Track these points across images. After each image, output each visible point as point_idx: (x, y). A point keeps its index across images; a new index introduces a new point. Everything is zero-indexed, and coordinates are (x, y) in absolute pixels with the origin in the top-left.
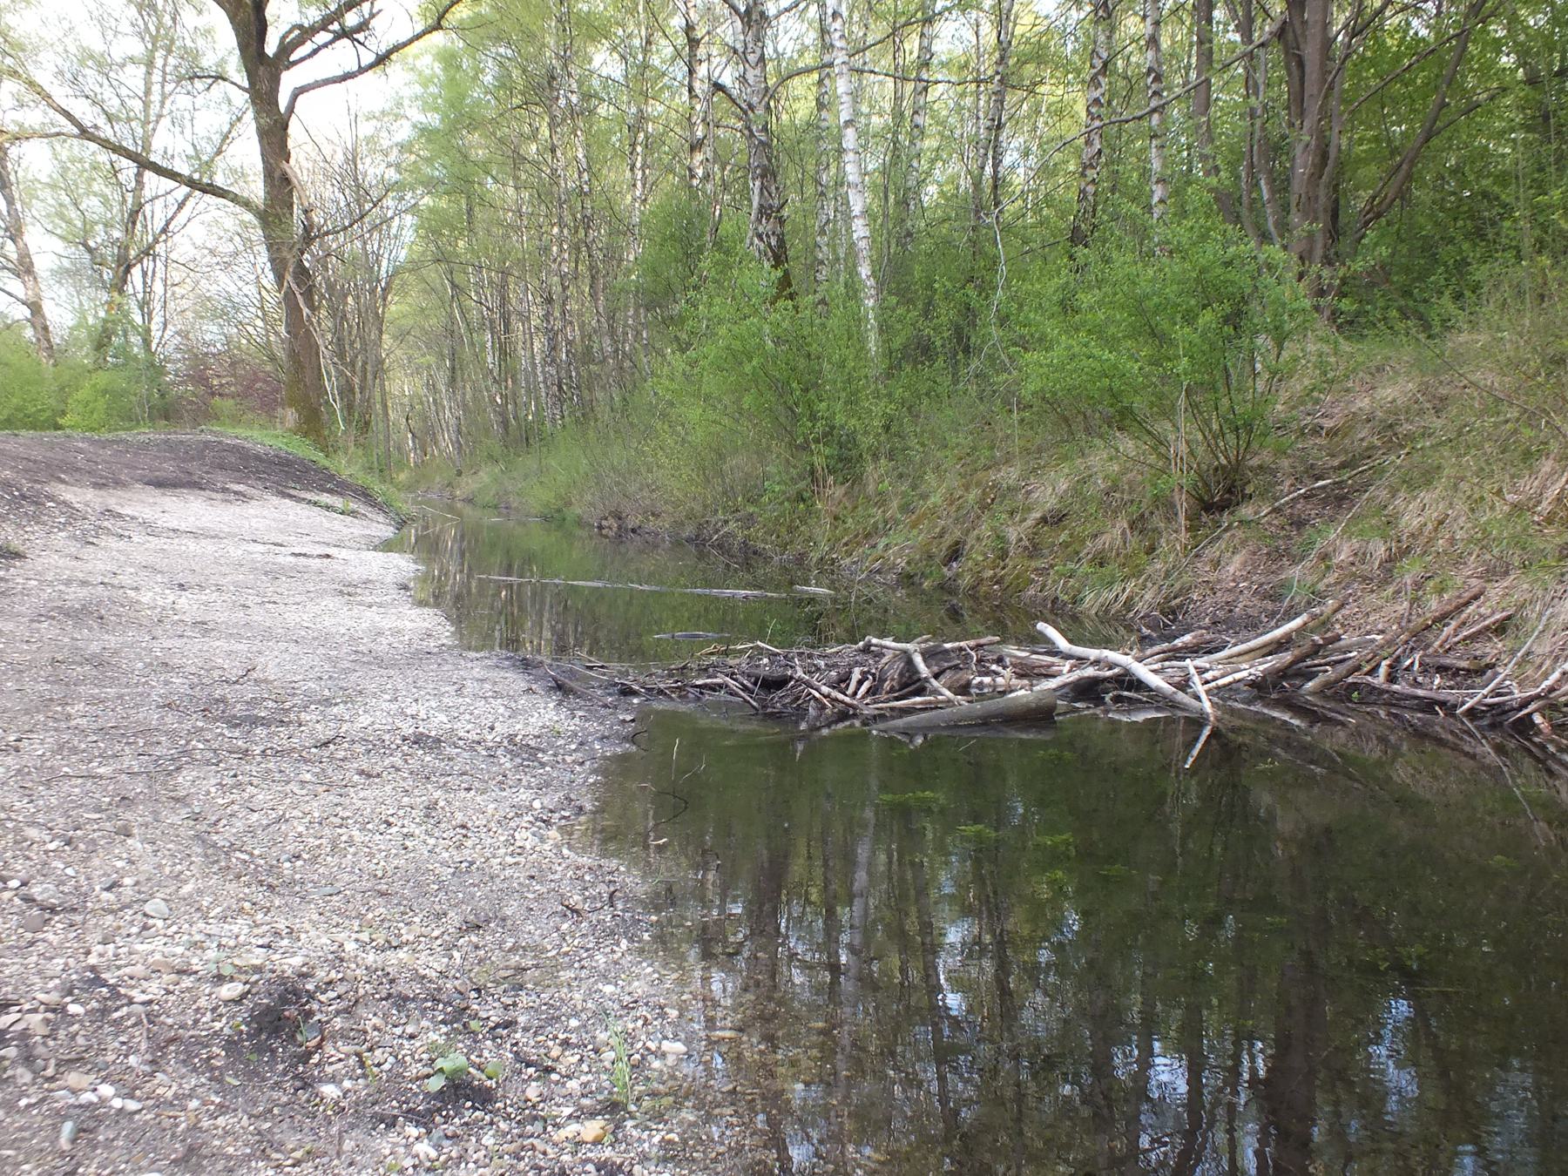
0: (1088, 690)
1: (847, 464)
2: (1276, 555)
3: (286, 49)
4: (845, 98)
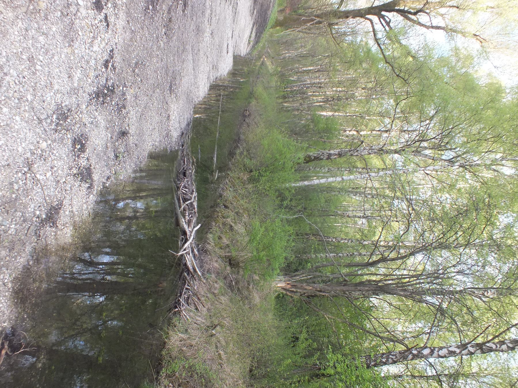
0: (184, 233)
1: (252, 180)
2: (218, 273)
3: (383, 17)
4: (349, 178)
